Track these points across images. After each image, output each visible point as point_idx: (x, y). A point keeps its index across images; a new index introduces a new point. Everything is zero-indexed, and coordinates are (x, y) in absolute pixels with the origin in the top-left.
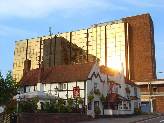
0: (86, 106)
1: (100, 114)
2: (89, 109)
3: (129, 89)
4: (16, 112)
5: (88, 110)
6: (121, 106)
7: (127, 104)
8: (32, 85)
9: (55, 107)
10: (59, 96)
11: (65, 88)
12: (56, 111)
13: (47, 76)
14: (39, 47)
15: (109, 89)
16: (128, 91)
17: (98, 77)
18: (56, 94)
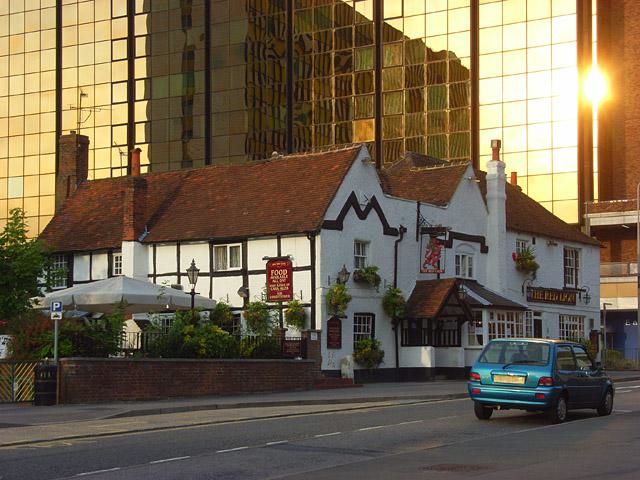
0: (319, 332)
1: (382, 366)
2: (329, 346)
3: (534, 258)
4: (50, 355)
5: (324, 351)
6: (478, 331)
7: (506, 322)
8: (100, 251)
9: (187, 339)
10: (211, 297)
11: (234, 263)
12: (192, 351)
13: (162, 209)
14: (122, 28)
15: (423, 262)
16: (525, 265)
17: (373, 214)
18: (193, 290)
